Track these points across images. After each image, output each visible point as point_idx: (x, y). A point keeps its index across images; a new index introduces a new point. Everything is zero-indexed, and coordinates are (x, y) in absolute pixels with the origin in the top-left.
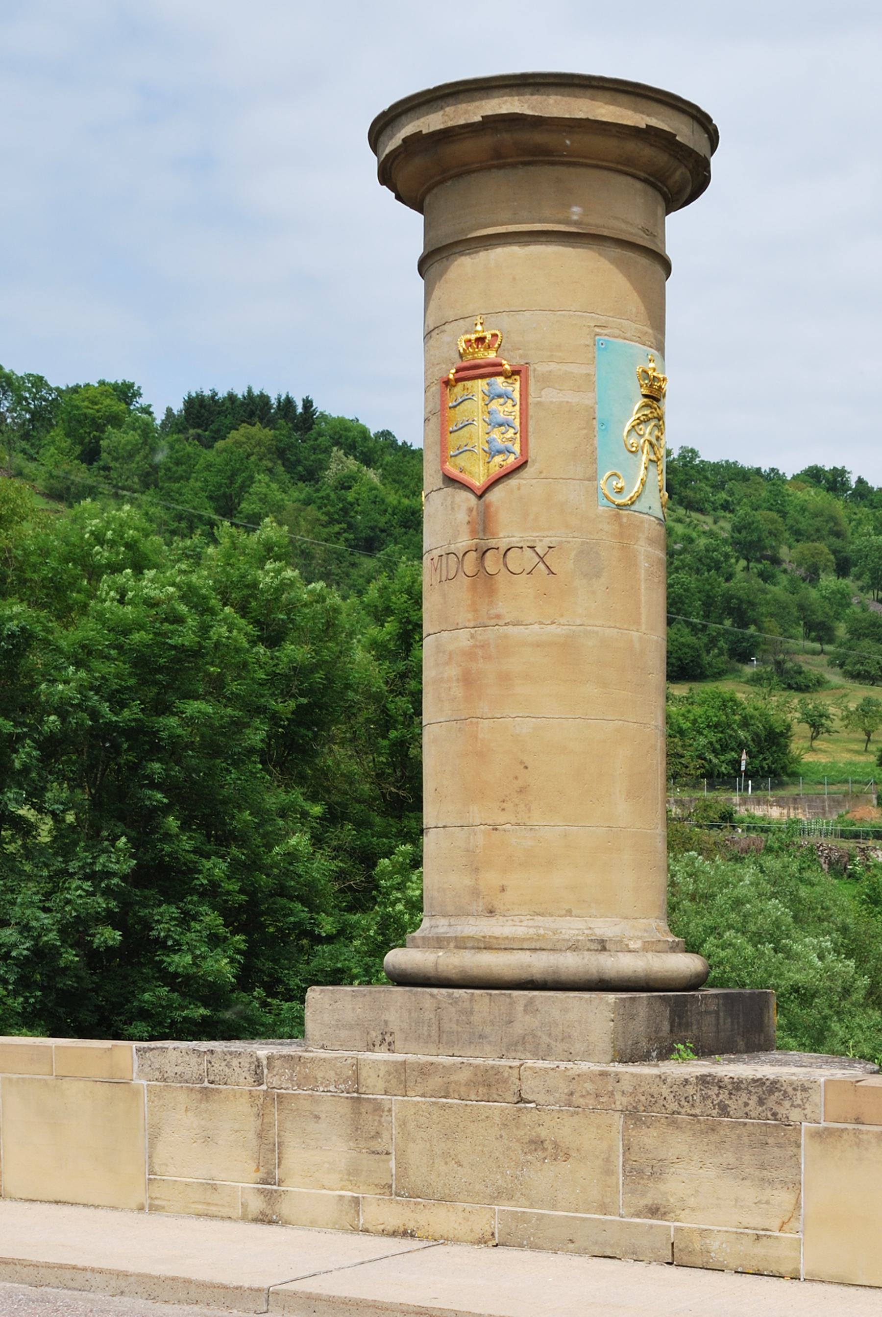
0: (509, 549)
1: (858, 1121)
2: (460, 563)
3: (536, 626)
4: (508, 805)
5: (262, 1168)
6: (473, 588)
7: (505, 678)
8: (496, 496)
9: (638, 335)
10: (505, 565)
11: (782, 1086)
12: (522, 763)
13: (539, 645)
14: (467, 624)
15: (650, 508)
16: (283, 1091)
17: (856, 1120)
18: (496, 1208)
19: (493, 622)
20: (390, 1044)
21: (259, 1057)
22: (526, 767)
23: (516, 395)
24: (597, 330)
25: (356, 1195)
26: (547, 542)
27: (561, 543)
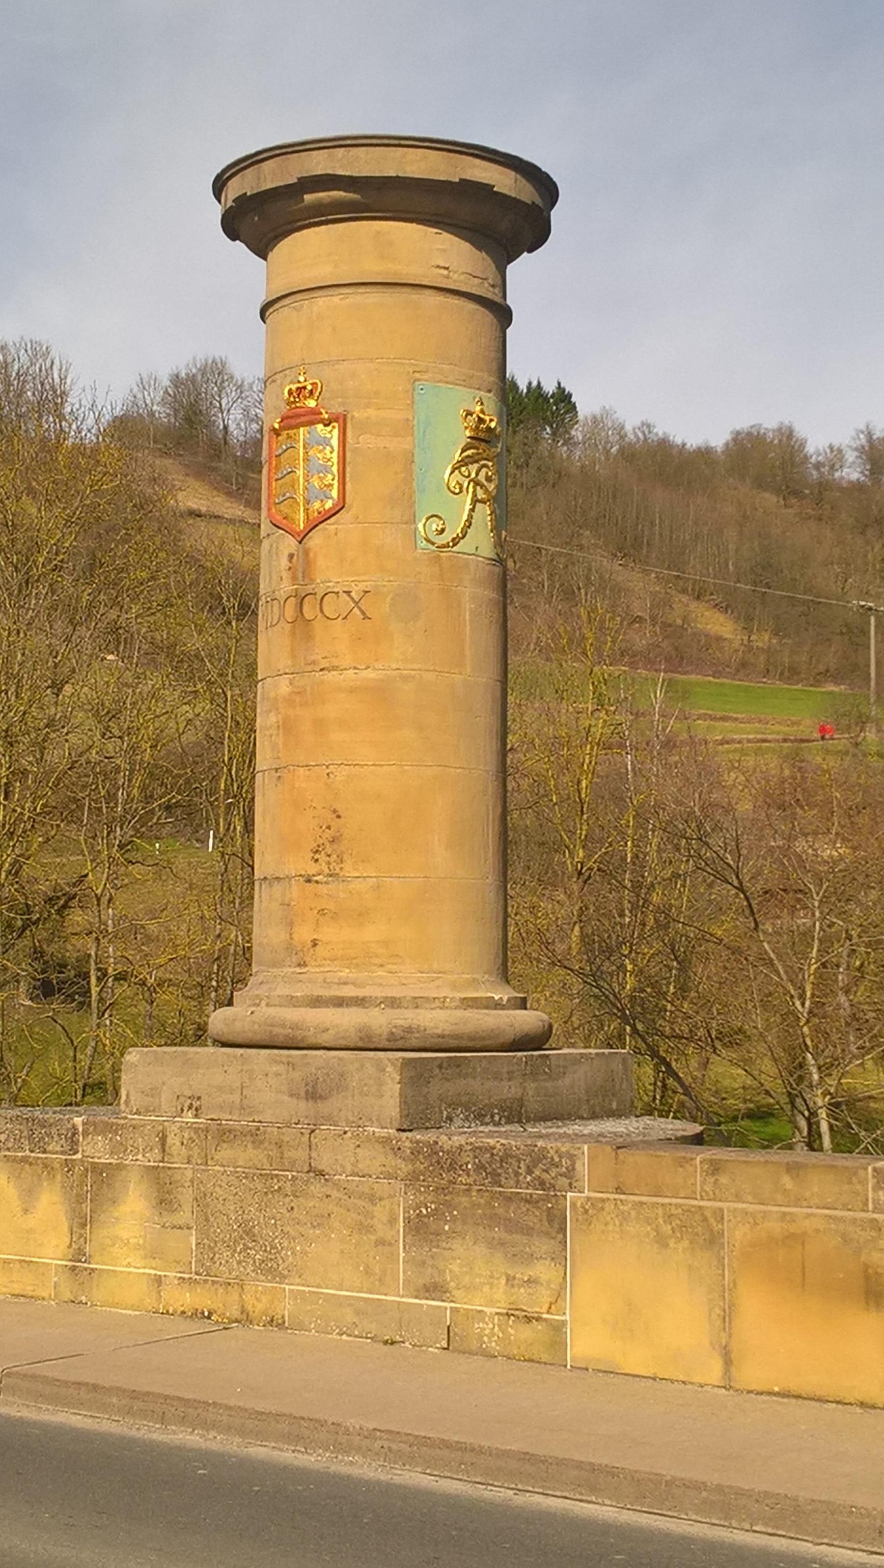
0: (326, 594)
1: (619, 1190)
2: (282, 608)
3: (352, 671)
4: (322, 857)
5: (74, 1245)
6: (293, 634)
7: (320, 726)
8: (315, 540)
9: (464, 378)
10: (321, 611)
11: (548, 1152)
12: (335, 811)
13: (353, 690)
14: (287, 671)
15: (477, 548)
16: (96, 1160)
17: (617, 1189)
18: (287, 1287)
19: (309, 668)
20: (197, 1110)
21: (76, 1123)
22: (339, 817)
23: (335, 442)
24: (417, 375)
25: (159, 1273)
26: (362, 586)
27: (377, 587)
